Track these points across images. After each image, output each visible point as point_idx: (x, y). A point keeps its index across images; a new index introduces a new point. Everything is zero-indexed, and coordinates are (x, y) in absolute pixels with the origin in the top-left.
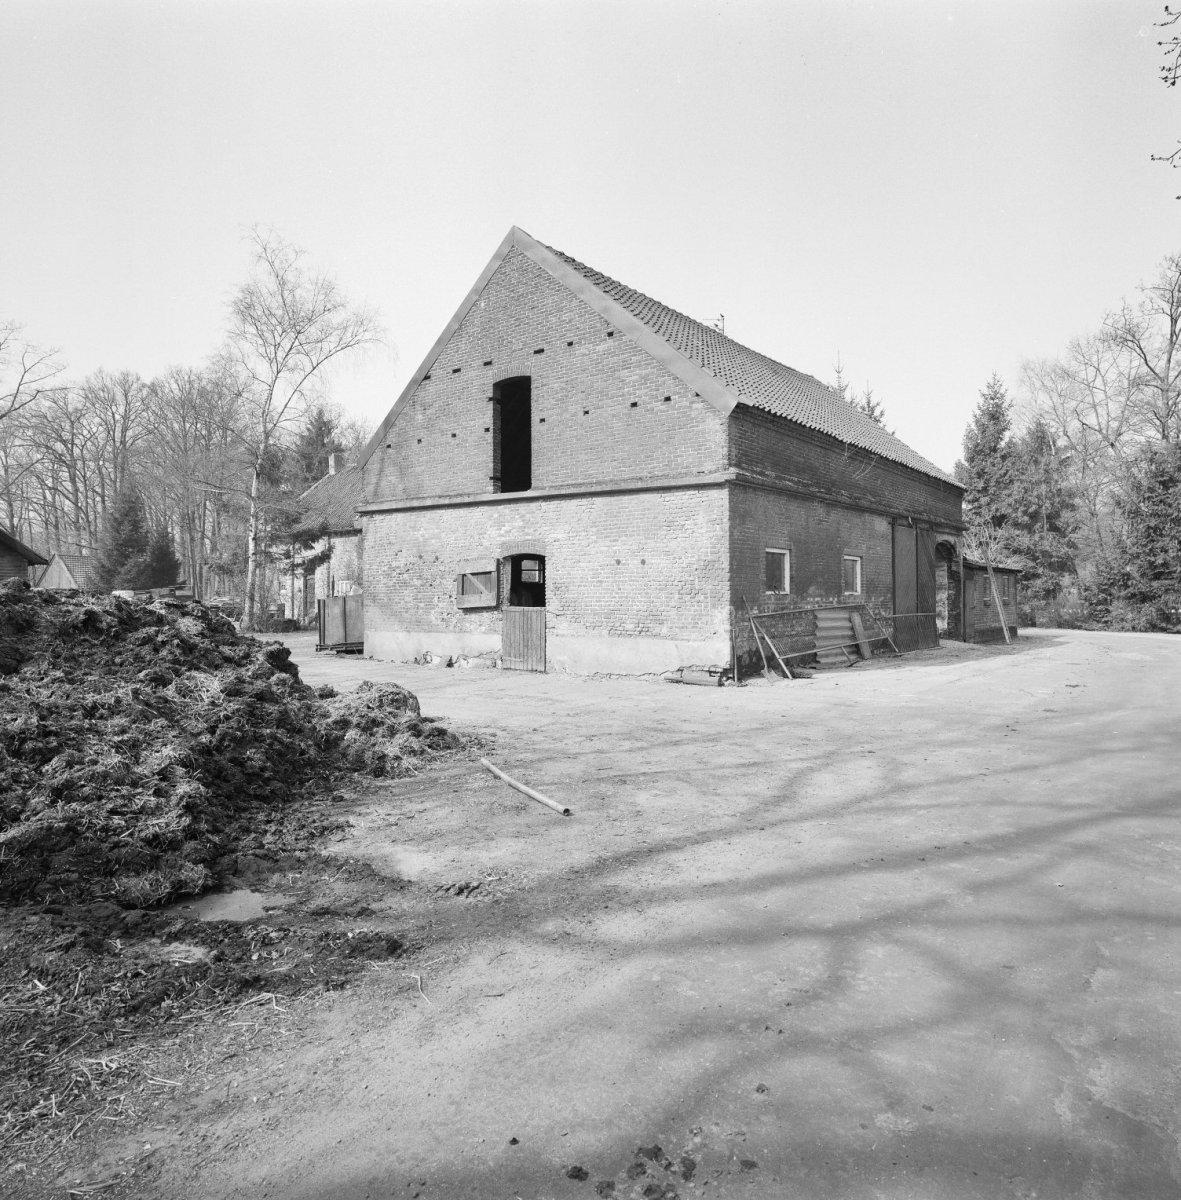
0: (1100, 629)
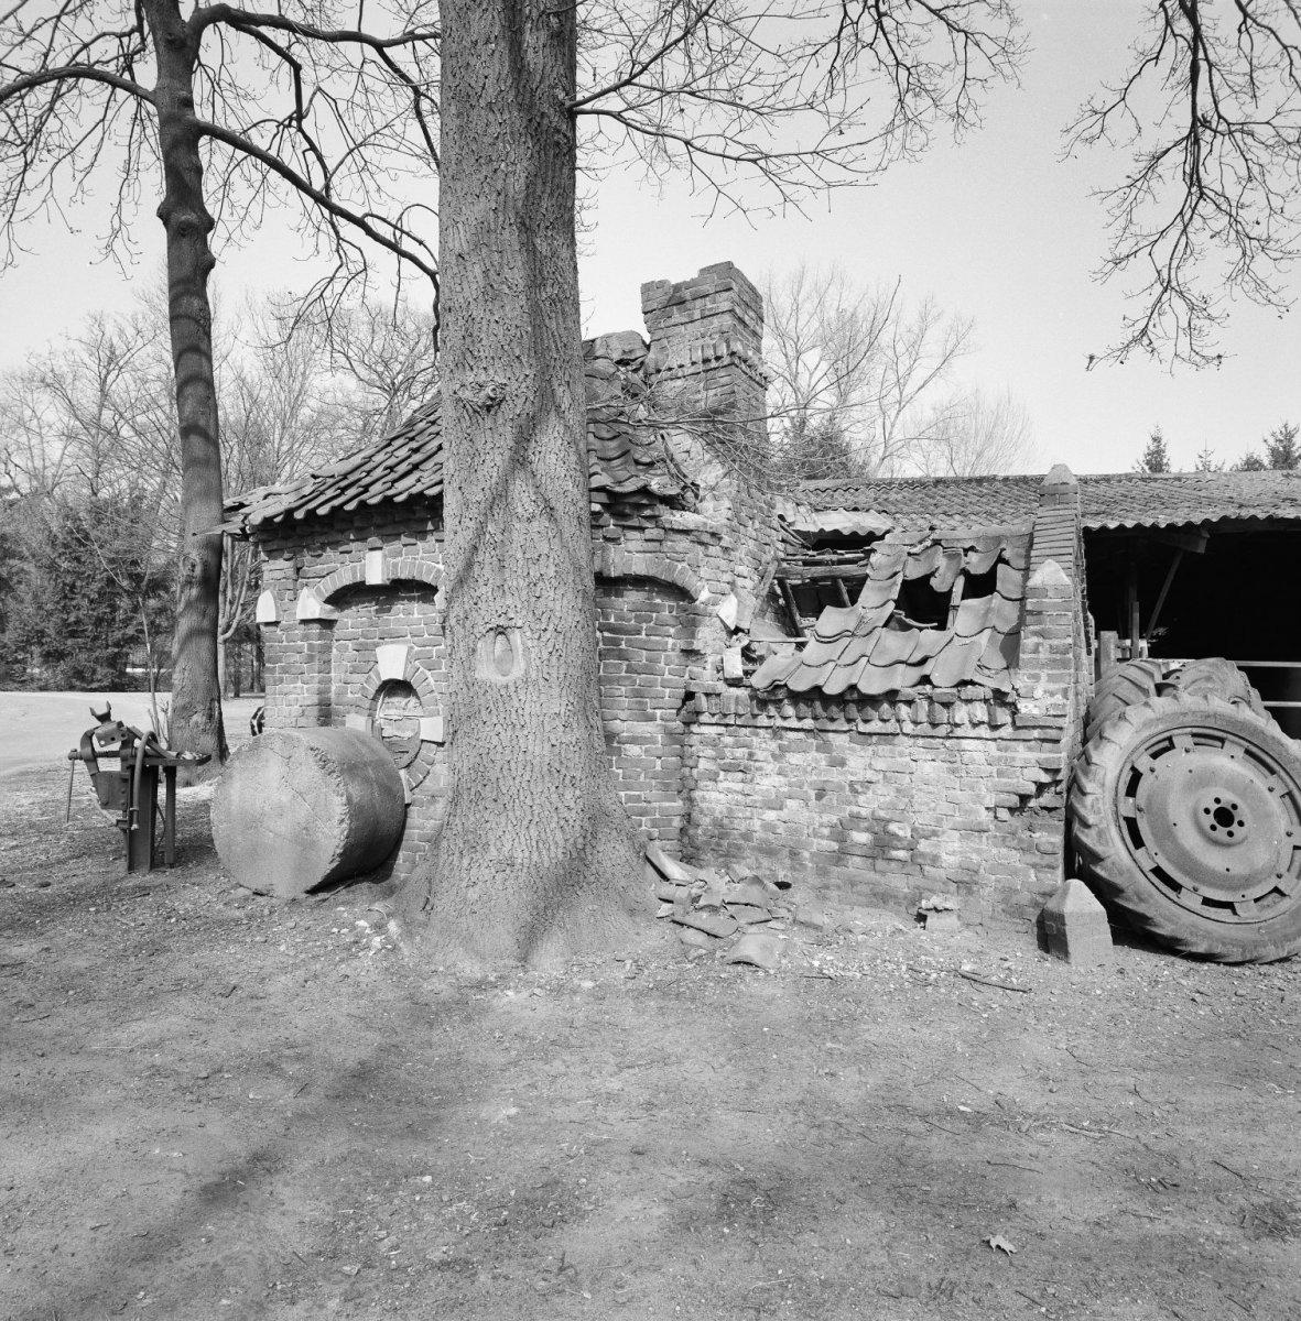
0: (17, 689)
